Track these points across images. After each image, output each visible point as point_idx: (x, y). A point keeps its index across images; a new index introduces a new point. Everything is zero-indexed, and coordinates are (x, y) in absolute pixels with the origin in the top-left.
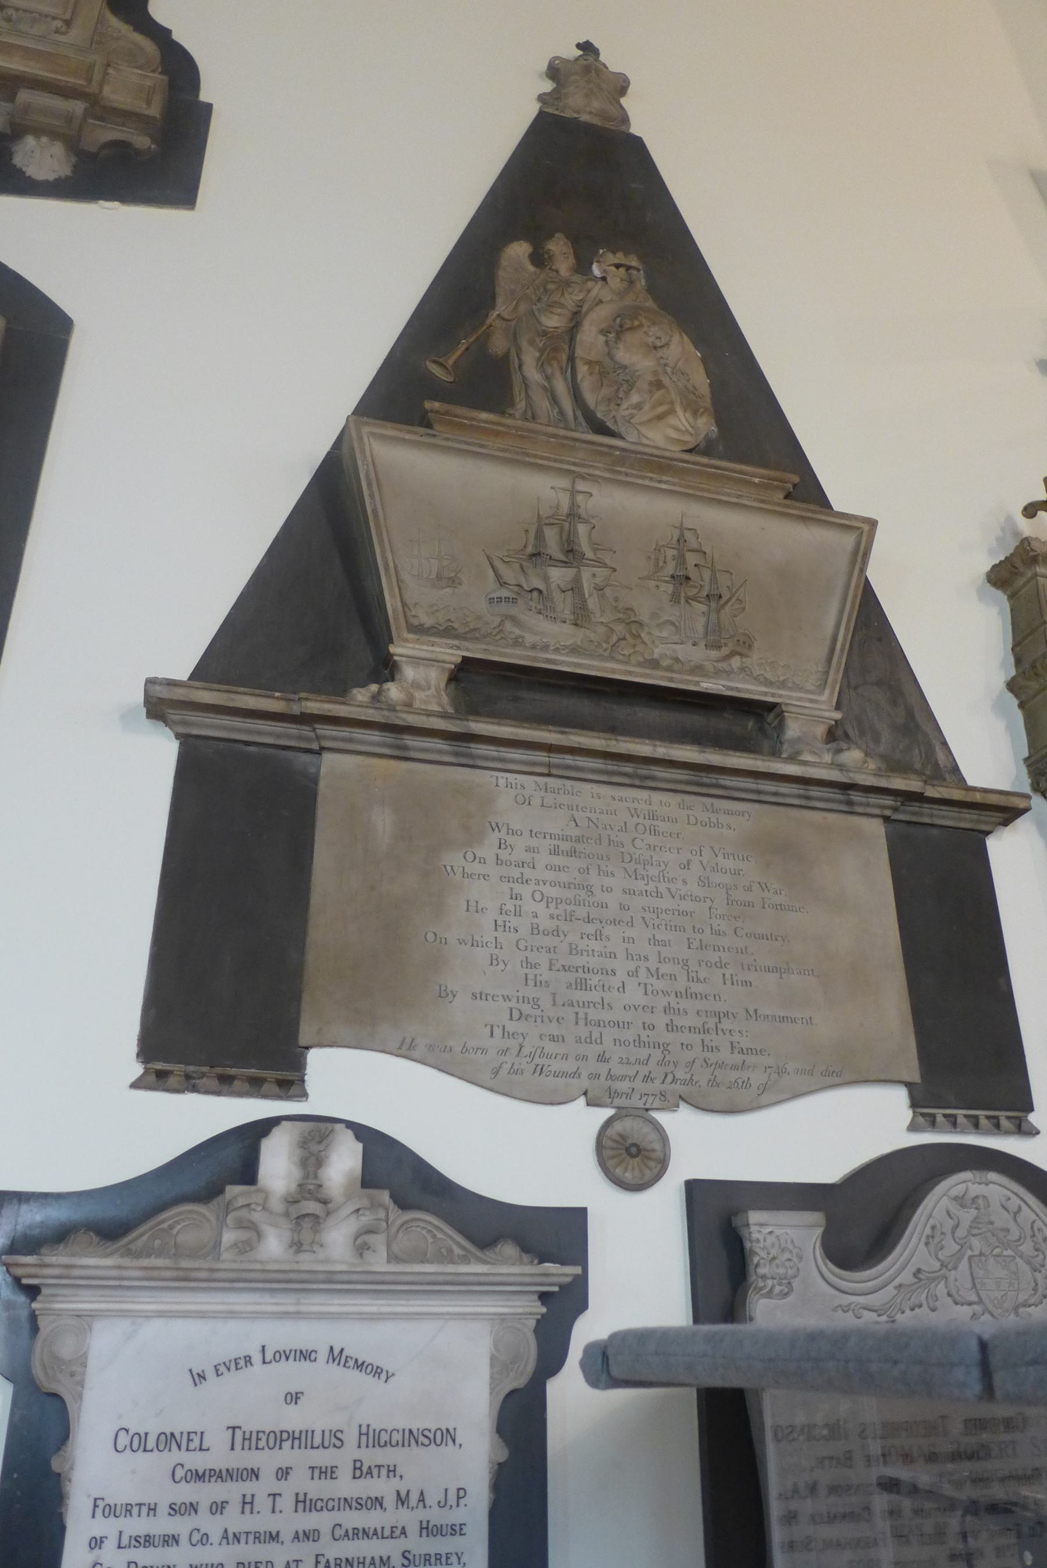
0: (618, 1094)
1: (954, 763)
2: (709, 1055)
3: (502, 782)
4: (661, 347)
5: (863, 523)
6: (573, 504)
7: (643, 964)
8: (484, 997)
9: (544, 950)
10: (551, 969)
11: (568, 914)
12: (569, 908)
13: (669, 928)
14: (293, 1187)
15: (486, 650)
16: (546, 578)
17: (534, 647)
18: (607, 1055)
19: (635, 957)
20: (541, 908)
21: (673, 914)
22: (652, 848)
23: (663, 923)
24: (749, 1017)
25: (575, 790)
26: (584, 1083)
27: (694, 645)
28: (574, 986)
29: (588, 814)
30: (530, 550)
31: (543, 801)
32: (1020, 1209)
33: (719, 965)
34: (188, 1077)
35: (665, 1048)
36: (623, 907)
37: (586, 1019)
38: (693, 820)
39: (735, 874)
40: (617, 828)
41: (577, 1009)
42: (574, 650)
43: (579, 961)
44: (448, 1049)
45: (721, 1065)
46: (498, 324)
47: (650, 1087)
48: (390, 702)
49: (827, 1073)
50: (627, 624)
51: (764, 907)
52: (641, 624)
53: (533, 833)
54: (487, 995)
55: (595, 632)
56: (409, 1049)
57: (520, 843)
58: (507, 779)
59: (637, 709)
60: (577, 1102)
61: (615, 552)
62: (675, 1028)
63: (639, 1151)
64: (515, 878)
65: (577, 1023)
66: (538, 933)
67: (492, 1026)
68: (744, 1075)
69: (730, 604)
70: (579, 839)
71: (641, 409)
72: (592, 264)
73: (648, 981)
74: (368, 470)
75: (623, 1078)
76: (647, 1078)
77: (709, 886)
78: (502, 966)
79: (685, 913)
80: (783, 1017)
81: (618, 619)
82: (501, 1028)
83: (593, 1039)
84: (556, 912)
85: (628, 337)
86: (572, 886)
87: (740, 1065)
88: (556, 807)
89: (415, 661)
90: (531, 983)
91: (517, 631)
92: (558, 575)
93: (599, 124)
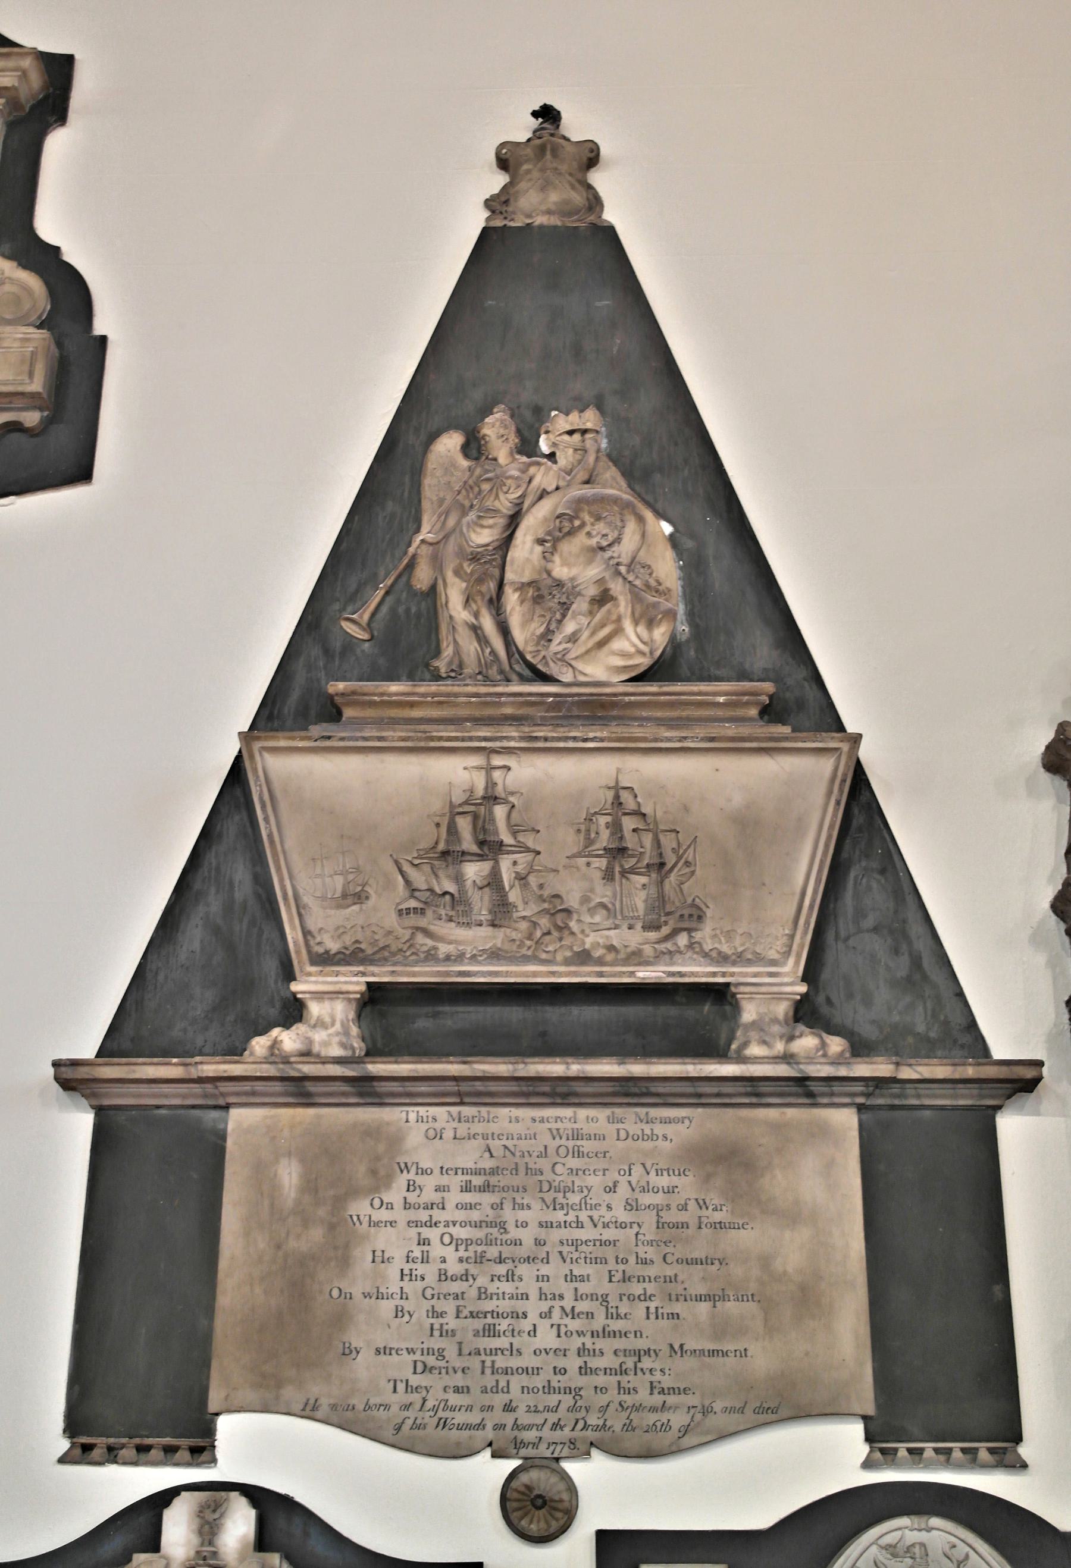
0: (524, 1444)
1: (971, 1018)
2: (626, 1397)
3: (412, 1117)
4: (610, 545)
5: (842, 741)
6: (491, 784)
7: (557, 1304)
8: (388, 1352)
9: (452, 1297)
10: (458, 1317)
11: (478, 1254)
12: (480, 1249)
13: (588, 1261)
14: (192, 1553)
15: (393, 972)
16: (459, 879)
17: (448, 958)
18: (514, 1404)
19: (549, 1297)
20: (449, 1252)
21: (595, 1245)
22: (574, 1172)
23: (583, 1255)
24: (673, 1354)
25: (491, 1116)
26: (489, 1434)
27: (629, 928)
28: (481, 1333)
29: (504, 1142)
30: (441, 846)
31: (455, 1132)
32: (967, 1557)
33: (642, 1298)
34: (110, 1449)
35: (576, 1392)
36: (539, 1243)
37: (493, 1366)
38: (623, 1135)
39: (669, 1192)
40: (535, 1154)
41: (483, 1357)
42: (495, 955)
43: (489, 1305)
44: (350, 1407)
45: (638, 1408)
46: (425, 550)
47: (558, 1435)
48: (283, 1054)
49: (760, 1410)
50: (553, 914)
51: (700, 1228)
52: (568, 911)
53: (444, 1170)
54: (391, 1349)
55: (516, 930)
56: (313, 1410)
57: (429, 1183)
58: (418, 1112)
59: (573, 1008)
60: (482, 1454)
61: (538, 831)
62: (589, 1370)
63: (545, 1503)
64: (424, 1222)
65: (483, 1373)
66: (446, 1280)
67: (395, 1381)
68: (664, 1417)
69: (676, 870)
70: (494, 1172)
71: (576, 640)
72: (539, 437)
73: (562, 1322)
74: (261, 791)
75: (529, 1427)
76: (556, 1426)
77: (637, 1210)
78: (407, 1317)
79: (607, 1243)
80: (713, 1350)
81: (542, 911)
82: (404, 1382)
83: (500, 1388)
84: (466, 1255)
85: (566, 547)
86: (484, 1224)
87: (661, 1406)
88: (469, 1139)
89: (319, 996)
90: (436, 1333)
91: (430, 943)
92: (474, 871)
93: (559, 224)
